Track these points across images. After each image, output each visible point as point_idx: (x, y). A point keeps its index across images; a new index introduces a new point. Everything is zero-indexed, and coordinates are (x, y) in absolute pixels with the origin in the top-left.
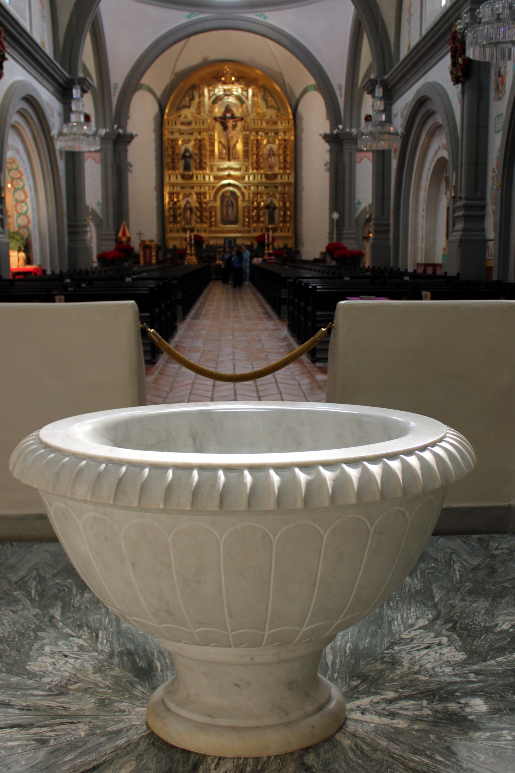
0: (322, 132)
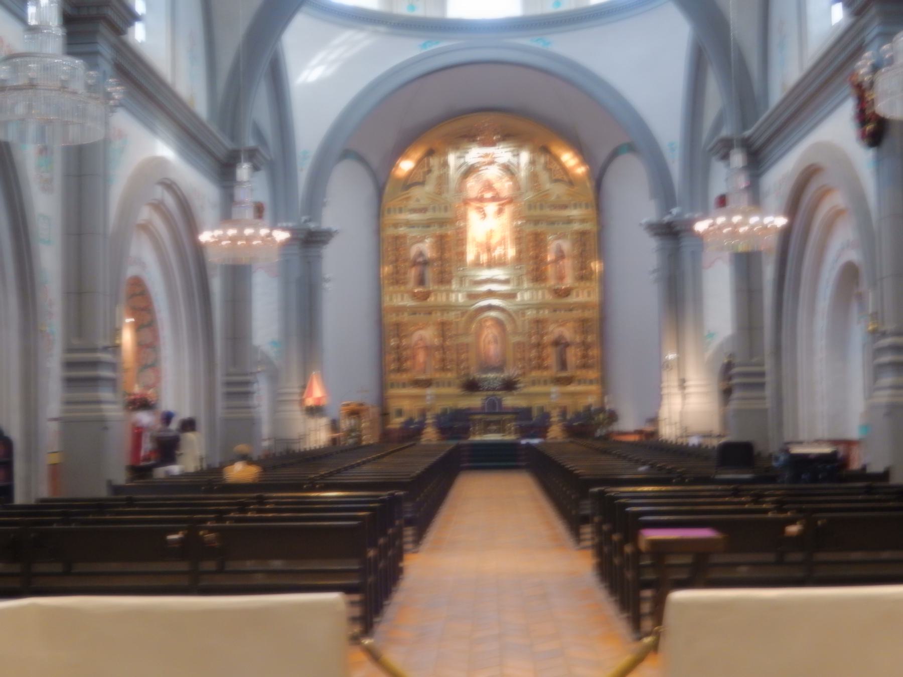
0: (645, 220)
